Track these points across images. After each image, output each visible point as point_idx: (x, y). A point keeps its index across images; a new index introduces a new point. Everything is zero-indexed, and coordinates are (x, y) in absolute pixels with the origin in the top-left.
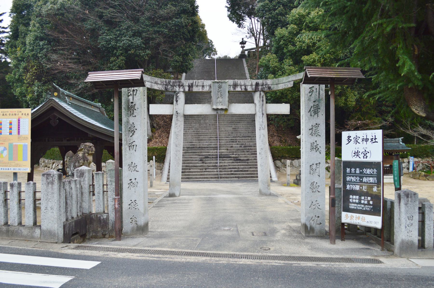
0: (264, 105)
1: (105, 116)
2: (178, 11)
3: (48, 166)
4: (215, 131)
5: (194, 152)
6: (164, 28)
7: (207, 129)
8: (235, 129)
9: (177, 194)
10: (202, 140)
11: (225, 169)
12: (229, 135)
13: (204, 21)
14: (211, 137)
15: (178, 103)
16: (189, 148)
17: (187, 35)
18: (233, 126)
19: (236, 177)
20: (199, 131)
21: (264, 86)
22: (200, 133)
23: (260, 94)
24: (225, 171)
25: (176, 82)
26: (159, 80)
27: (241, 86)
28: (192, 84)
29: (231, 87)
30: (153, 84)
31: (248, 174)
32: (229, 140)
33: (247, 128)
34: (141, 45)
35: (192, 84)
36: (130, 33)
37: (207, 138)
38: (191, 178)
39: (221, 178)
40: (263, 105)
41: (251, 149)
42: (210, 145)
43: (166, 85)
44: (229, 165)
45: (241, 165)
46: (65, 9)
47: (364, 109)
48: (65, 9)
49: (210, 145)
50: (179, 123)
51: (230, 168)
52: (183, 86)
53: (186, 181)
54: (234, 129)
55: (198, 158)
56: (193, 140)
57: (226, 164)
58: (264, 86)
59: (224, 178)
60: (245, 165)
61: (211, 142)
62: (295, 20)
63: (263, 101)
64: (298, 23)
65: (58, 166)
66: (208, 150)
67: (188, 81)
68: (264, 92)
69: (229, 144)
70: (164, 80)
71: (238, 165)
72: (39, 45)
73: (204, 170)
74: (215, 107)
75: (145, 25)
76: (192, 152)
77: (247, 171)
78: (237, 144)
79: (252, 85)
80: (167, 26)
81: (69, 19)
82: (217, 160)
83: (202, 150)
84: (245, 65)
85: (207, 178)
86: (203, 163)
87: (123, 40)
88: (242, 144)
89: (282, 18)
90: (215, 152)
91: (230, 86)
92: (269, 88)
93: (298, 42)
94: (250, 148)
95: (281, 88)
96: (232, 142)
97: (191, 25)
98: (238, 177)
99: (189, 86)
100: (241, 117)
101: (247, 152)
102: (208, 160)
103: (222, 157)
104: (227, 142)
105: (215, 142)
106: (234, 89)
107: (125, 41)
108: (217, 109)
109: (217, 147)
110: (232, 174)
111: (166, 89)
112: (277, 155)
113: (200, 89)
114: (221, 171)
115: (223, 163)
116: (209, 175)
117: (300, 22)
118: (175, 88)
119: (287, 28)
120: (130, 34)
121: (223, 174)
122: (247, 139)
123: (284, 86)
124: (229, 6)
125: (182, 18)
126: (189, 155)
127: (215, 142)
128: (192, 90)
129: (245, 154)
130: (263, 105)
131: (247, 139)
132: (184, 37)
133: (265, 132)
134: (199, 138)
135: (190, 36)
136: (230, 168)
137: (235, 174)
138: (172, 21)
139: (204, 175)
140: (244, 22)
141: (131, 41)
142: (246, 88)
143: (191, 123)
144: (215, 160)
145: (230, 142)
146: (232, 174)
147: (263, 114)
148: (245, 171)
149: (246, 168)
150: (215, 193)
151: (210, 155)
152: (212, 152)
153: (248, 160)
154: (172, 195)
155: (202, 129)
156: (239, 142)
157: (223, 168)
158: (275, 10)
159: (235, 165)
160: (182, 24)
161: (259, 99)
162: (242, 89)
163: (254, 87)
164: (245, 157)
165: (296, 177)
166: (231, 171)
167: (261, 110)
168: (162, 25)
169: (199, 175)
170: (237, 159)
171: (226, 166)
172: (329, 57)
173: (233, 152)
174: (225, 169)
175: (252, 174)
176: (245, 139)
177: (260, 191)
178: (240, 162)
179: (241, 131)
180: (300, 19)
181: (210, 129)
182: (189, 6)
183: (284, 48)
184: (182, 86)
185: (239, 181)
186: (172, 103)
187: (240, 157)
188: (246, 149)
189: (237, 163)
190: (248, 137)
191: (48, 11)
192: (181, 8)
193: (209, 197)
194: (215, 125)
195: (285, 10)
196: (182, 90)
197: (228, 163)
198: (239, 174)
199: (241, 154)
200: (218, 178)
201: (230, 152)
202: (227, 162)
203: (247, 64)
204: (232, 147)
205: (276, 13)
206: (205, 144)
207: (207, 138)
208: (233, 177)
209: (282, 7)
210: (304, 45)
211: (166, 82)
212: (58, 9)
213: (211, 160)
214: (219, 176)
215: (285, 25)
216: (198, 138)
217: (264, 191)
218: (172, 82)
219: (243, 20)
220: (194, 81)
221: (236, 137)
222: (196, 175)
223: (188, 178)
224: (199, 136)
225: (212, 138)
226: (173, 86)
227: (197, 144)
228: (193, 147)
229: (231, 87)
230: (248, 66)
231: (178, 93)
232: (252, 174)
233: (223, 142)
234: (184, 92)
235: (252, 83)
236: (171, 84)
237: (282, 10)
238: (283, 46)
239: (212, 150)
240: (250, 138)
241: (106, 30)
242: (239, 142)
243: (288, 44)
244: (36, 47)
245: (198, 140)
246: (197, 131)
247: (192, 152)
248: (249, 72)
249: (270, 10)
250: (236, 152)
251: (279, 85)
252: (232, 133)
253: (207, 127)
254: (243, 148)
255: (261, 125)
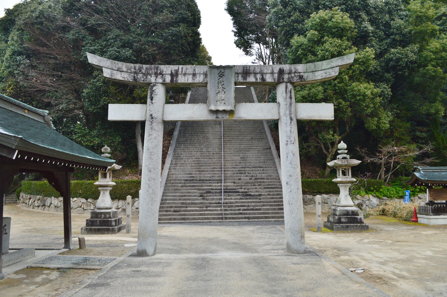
0: (293, 105)
1: (51, 127)
2: (176, 19)
3: (25, 202)
4: (219, 161)
5: (193, 186)
6: (159, 38)
7: (210, 159)
8: (244, 158)
9: (150, 250)
10: (203, 171)
11: (232, 206)
12: (237, 165)
13: (210, 54)
14: (214, 168)
15: (154, 101)
16: (187, 180)
17: (186, 48)
18: (242, 155)
19: (245, 218)
20: (199, 161)
21: (293, 75)
22: (201, 163)
23: (286, 87)
24: (231, 210)
25: (151, 69)
26: (124, 66)
27: (255, 74)
28: (177, 71)
29: (240, 76)
30: (115, 72)
31: (261, 214)
32: (236, 171)
33: (258, 158)
34: (130, 56)
35: (177, 71)
36: (119, 43)
37: (210, 168)
38: (188, 219)
39: (226, 218)
40: (291, 104)
41: (263, 182)
42: (213, 176)
43: (135, 73)
44: (237, 202)
45: (251, 202)
46: (44, 17)
47: (396, 134)
48: (44, 17)
49: (213, 176)
50: (155, 134)
51: (238, 206)
52: (163, 75)
53: (181, 223)
54: (242, 158)
55: (198, 193)
56: (193, 171)
57: (232, 201)
58: (293, 75)
59: (230, 218)
60: (257, 202)
61: (214, 174)
62: (316, 25)
63: (291, 98)
64: (318, 29)
65: (34, 202)
66: (211, 183)
67: (171, 66)
68: (292, 83)
69: (237, 176)
70: (132, 65)
71: (248, 202)
72: (16, 61)
73: (205, 209)
74: (213, 108)
75: (136, 35)
76: (190, 186)
77: (260, 209)
78: (247, 176)
79: (272, 73)
80: (162, 36)
81: (48, 28)
82: (221, 195)
83: (204, 183)
84: (253, 93)
85: (208, 219)
86: (203, 199)
87: (110, 51)
88: (252, 176)
89: (300, 26)
90: (218, 186)
91: (238, 74)
92: (301, 77)
93: (320, 51)
94: (262, 180)
95: (319, 78)
96: (240, 173)
97: (191, 36)
98: (248, 218)
99: (172, 75)
100: (256, 125)
101: (259, 185)
102: (210, 196)
103: (227, 191)
104: (234, 174)
105: (219, 174)
106: (245, 78)
107: (112, 52)
108: (216, 112)
109: (221, 180)
110: (241, 214)
111: (135, 79)
112: (310, 188)
113: (189, 79)
114: (226, 210)
115: (228, 199)
116: (211, 214)
117: (323, 28)
118: (149, 77)
119: (305, 36)
120: (118, 44)
121: (228, 214)
122: (258, 170)
123: (324, 75)
124: (235, 30)
125: (181, 26)
126: (187, 190)
127: (219, 174)
128: (176, 81)
129: (256, 188)
130: (291, 104)
131: (258, 170)
132: (182, 49)
133: (295, 148)
134: (200, 168)
135: (190, 49)
136: (238, 206)
137: (244, 214)
138: (169, 30)
139: (204, 214)
140: (251, 50)
141: (119, 52)
142: (263, 77)
143: (192, 152)
144: (219, 195)
145: (237, 173)
146: (241, 214)
147: (291, 119)
148: (257, 210)
149: (258, 206)
150: (214, 247)
151: (212, 189)
152: (215, 185)
153: (260, 195)
154: (141, 253)
155: (204, 158)
156: (248, 173)
157: (228, 205)
158: (290, 17)
159: (244, 202)
160: (181, 33)
161: (284, 94)
162: (256, 79)
163: (276, 76)
164: (257, 192)
165: (328, 218)
166: (239, 210)
167: (288, 112)
168: (157, 34)
169: (197, 215)
170: (246, 195)
171: (233, 203)
172: (358, 69)
173: (241, 186)
174: (232, 206)
175: (266, 213)
176: (256, 170)
177: (288, 246)
178: (250, 198)
179: (251, 160)
180: (321, 24)
181: (214, 158)
182: (190, 14)
183: (302, 58)
184: (160, 74)
185: (249, 224)
186: (145, 103)
187: (251, 192)
188: (257, 182)
189: (247, 199)
190: (259, 167)
191: (25, 20)
192: (179, 16)
193: (203, 259)
194: (219, 154)
195: (303, 16)
196: (160, 80)
197: (235, 199)
198: (250, 214)
199: (252, 188)
200: (222, 219)
201: (237, 186)
202: (233, 199)
203: (255, 91)
204: (240, 179)
205: (292, 20)
206: (207, 176)
207: (210, 168)
208: (242, 218)
209: (298, 14)
210: (327, 53)
211: (135, 68)
212: (37, 18)
213: (214, 196)
214: (224, 216)
215: (302, 33)
216: (198, 168)
217: (295, 246)
218: (144, 68)
219: (250, 47)
220: (181, 67)
221: (244, 168)
222: (194, 215)
223: (184, 219)
224: (199, 166)
225: (216, 168)
226: (146, 74)
227: (197, 176)
228: (192, 180)
229: (240, 76)
230: (256, 94)
231: (155, 85)
232: (266, 213)
233: (229, 174)
234: (164, 84)
235: (273, 70)
236: (144, 71)
237: (299, 17)
238: (302, 56)
239: (215, 183)
240: (261, 169)
241: (91, 40)
242: (248, 173)
243: (307, 53)
244: (13, 62)
245: (199, 171)
246: (197, 161)
247: (190, 186)
248: (258, 99)
249: (284, 17)
250: (245, 186)
251: (317, 73)
252: (240, 163)
253: (210, 156)
254: (254, 181)
255: (289, 137)
